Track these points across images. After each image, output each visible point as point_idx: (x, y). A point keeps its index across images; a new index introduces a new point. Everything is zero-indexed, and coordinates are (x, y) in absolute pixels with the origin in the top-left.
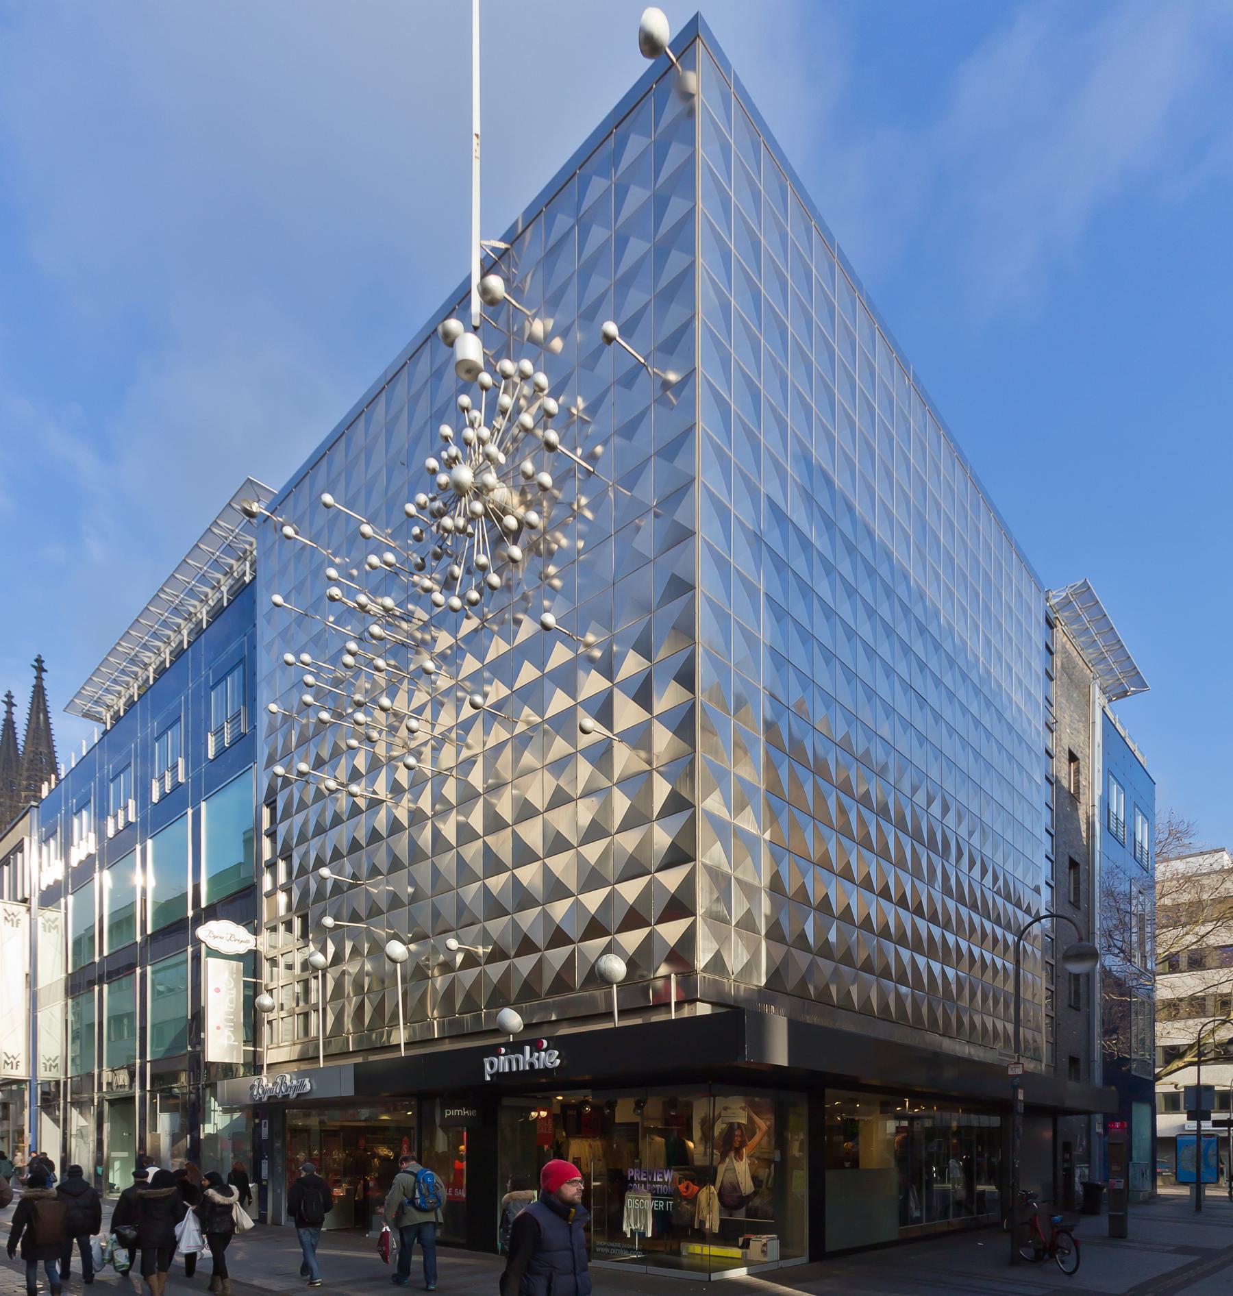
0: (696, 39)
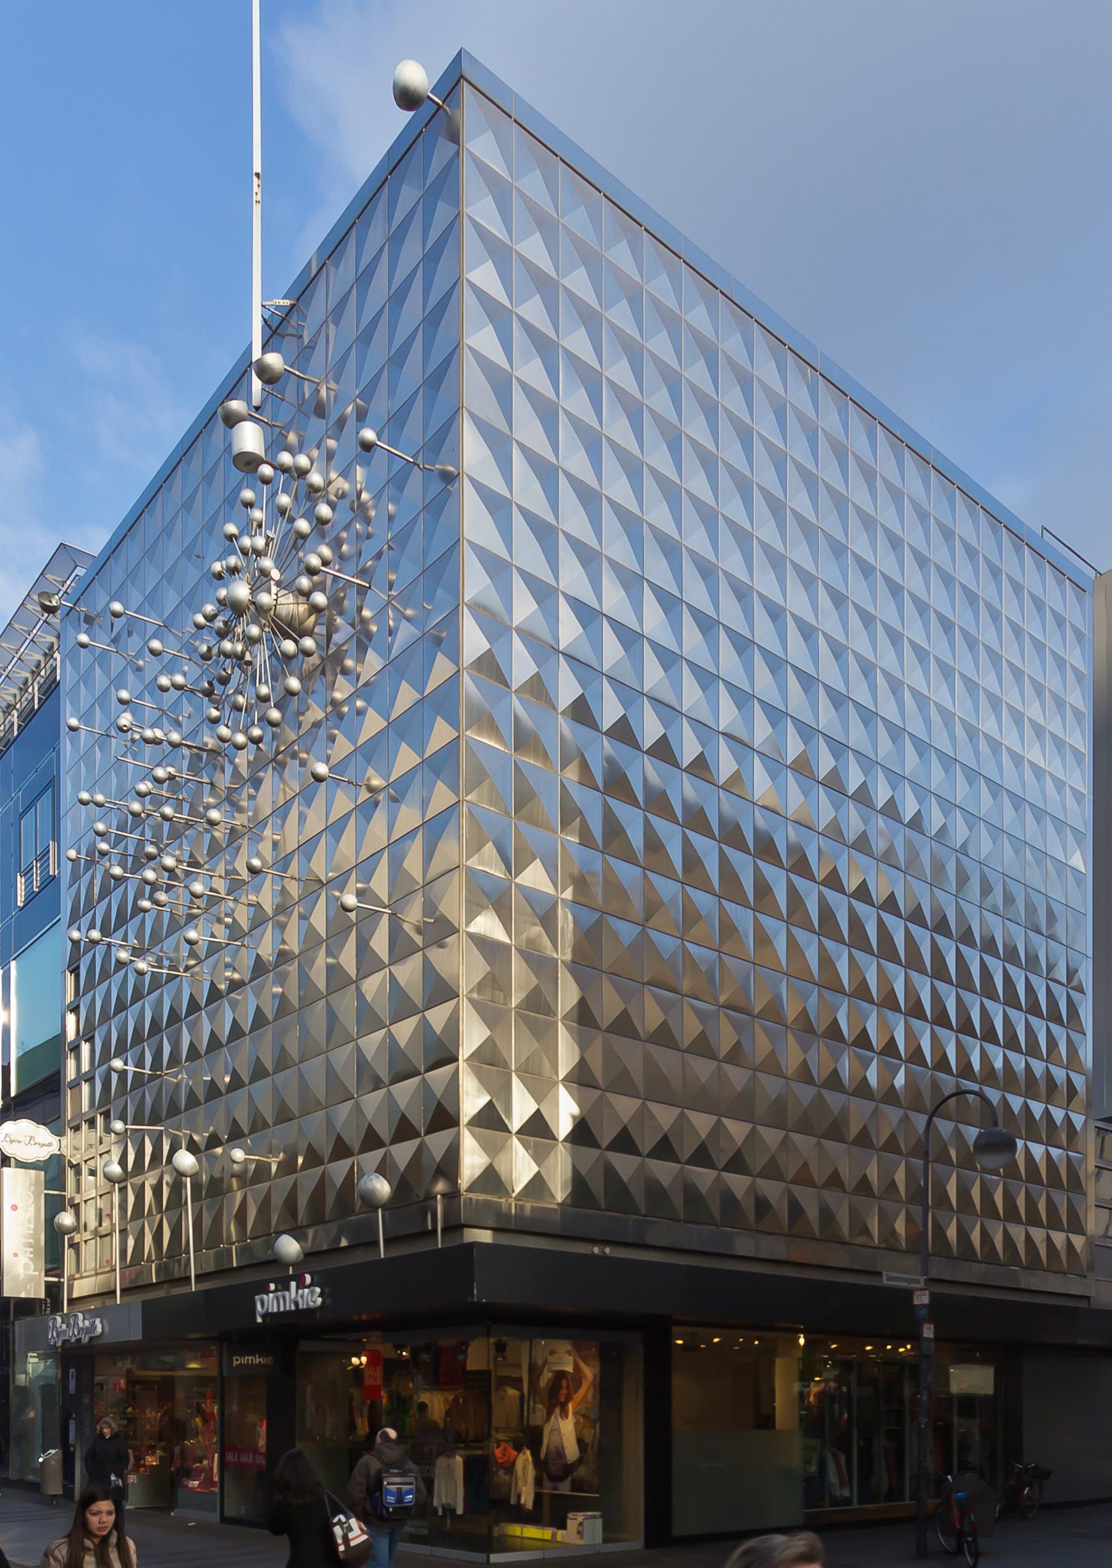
0: (459, 81)
